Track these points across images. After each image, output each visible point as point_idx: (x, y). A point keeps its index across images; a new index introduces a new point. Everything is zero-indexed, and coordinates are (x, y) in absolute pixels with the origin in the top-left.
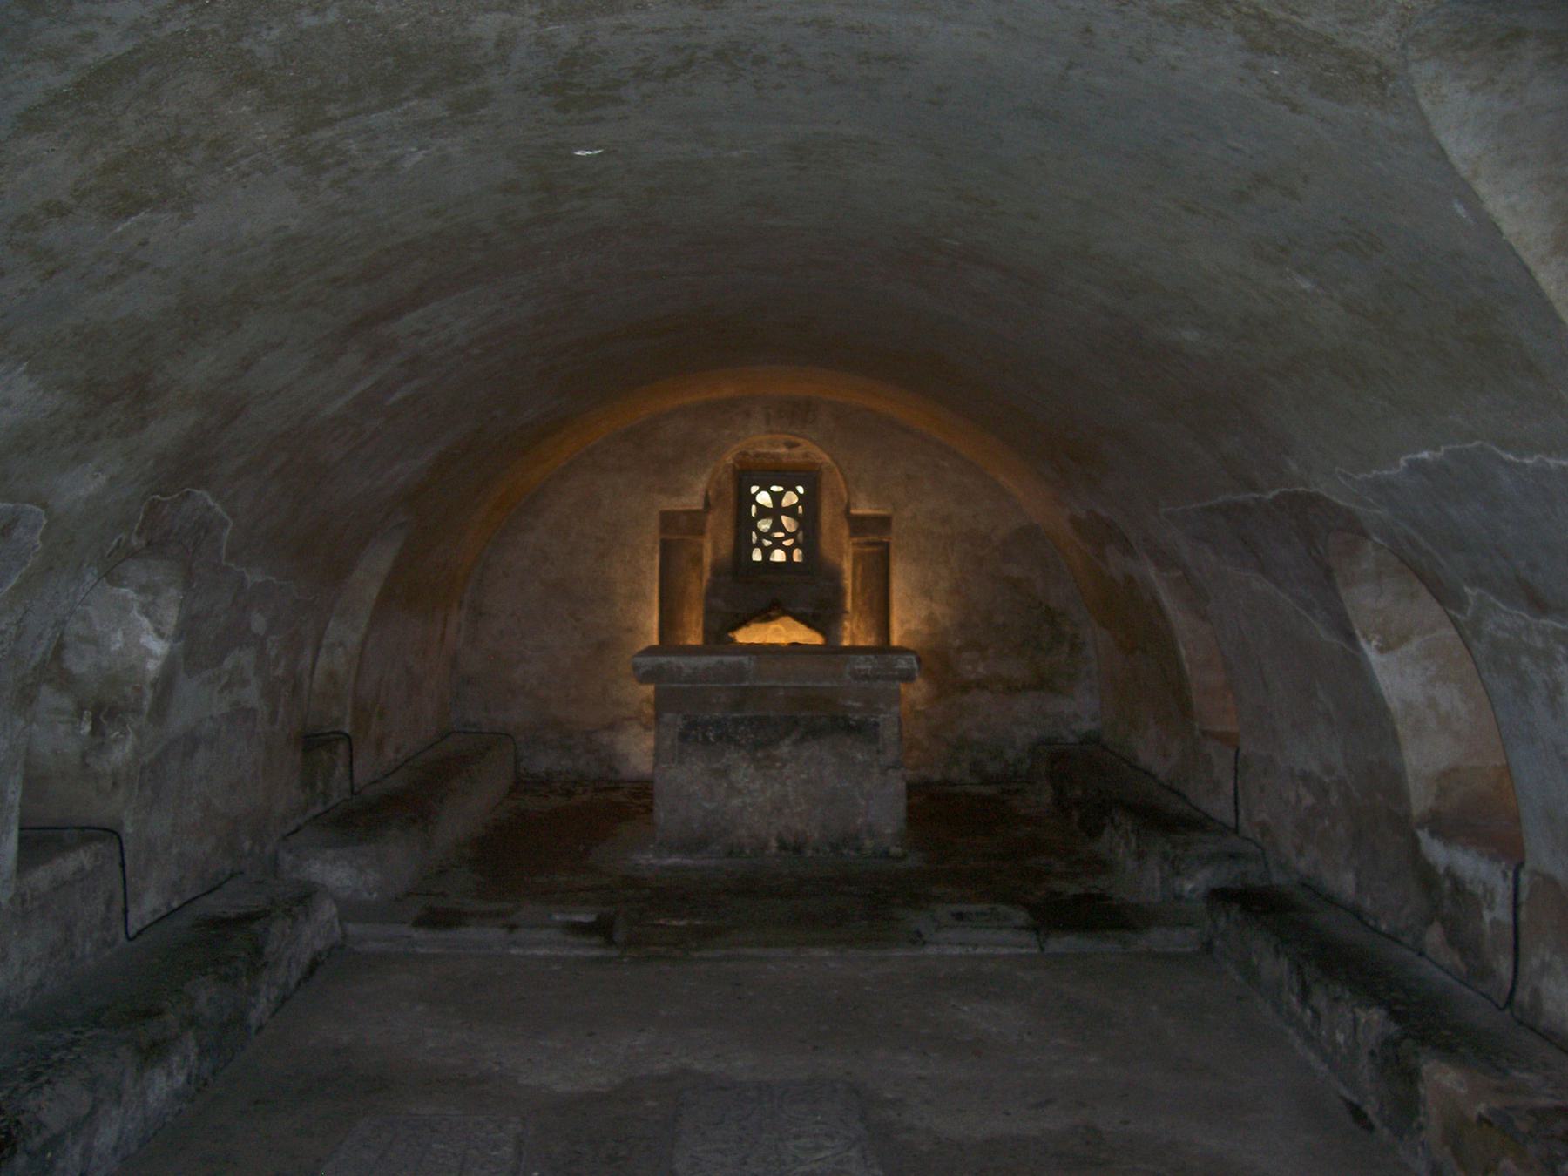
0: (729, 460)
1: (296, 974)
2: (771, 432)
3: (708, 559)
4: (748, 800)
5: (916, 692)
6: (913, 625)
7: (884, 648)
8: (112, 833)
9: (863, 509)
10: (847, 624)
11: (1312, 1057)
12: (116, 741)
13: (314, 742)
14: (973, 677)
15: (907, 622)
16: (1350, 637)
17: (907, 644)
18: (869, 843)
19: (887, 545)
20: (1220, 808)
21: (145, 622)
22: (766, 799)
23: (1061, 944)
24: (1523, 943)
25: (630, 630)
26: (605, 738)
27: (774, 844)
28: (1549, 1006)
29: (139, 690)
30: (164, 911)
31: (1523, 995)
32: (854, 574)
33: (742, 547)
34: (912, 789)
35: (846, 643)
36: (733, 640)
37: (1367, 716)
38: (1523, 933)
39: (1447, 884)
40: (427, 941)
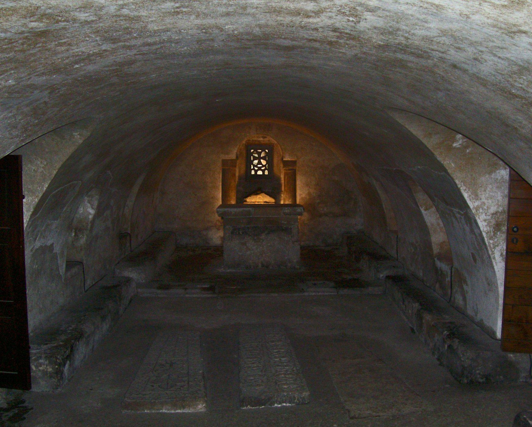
0: (244, 142)
1: (128, 302)
2: (258, 134)
3: (237, 174)
4: (252, 252)
5: (305, 217)
6: (304, 196)
7: (294, 205)
8: (81, 263)
9: (287, 158)
10: (282, 195)
11: (405, 318)
12: (81, 238)
13: (122, 237)
14: (323, 212)
15: (301, 195)
16: (418, 207)
17: (302, 204)
18: (289, 265)
19: (295, 170)
20: (393, 253)
21: (89, 205)
22: (257, 251)
23: (344, 292)
24: (453, 286)
25: (212, 198)
26: (204, 233)
27: (260, 265)
28: (456, 301)
29: (87, 223)
30: (91, 285)
31: (452, 299)
32: (285, 180)
33: (249, 170)
34: (302, 248)
35: (282, 203)
36: (246, 201)
37: (423, 228)
38: (453, 283)
39: (440, 272)
40: (161, 293)
